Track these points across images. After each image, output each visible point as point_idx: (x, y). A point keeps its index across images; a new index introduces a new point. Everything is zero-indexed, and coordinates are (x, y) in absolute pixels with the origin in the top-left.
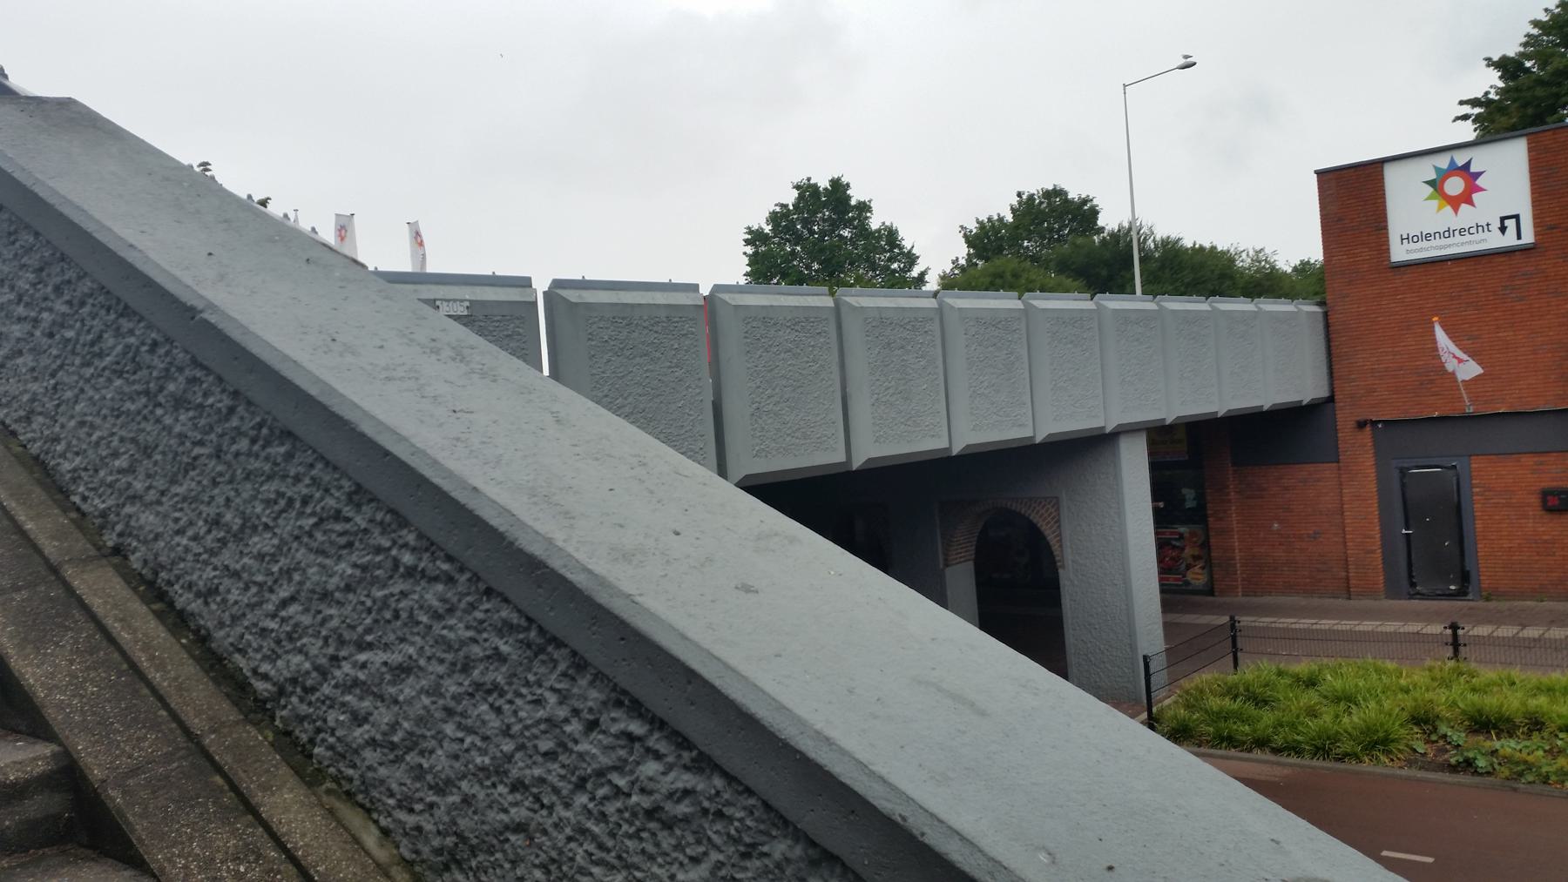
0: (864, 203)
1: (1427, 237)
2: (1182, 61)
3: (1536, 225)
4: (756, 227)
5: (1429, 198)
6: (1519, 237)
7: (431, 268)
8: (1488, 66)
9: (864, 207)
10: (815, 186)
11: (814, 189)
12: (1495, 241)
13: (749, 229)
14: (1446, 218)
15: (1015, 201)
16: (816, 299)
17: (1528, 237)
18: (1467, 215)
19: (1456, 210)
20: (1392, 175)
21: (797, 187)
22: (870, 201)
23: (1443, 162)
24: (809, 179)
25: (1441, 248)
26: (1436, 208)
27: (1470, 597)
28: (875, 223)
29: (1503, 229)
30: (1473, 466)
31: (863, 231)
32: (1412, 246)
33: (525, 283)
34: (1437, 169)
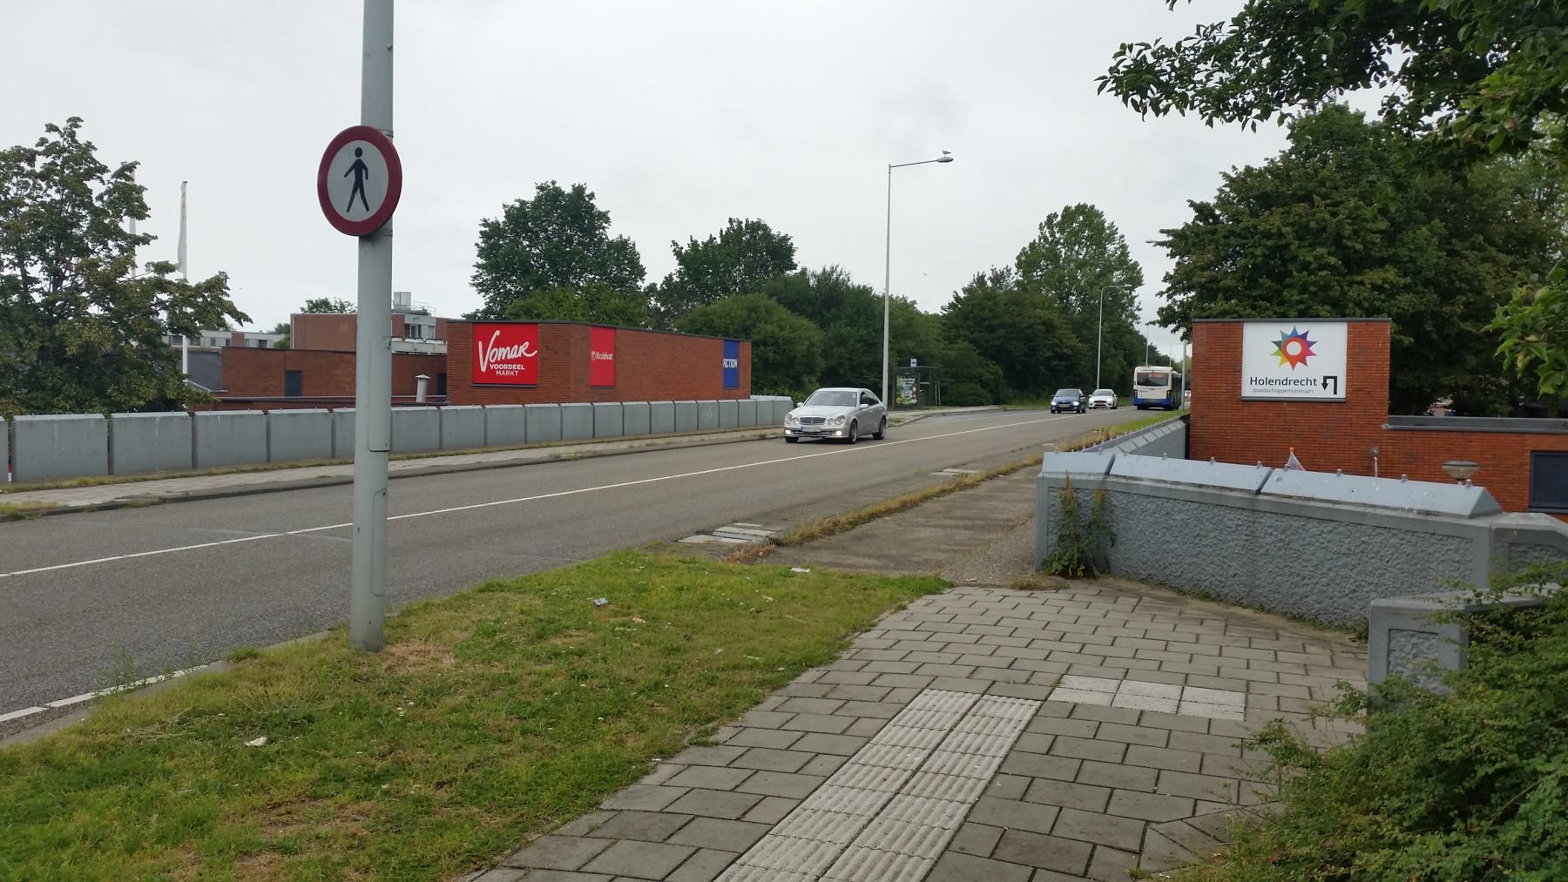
2: (942, 156)
3: (1347, 386)
4: (492, 220)
5: (1275, 354)
6: (1335, 393)
8: (1191, 206)
10: (557, 190)
11: (558, 193)
12: (1318, 393)
13: (485, 223)
14: (1284, 370)
15: (725, 226)
17: (1341, 394)
18: (1300, 371)
19: (1293, 366)
24: (553, 183)
29: (1325, 385)
32: (1258, 387)
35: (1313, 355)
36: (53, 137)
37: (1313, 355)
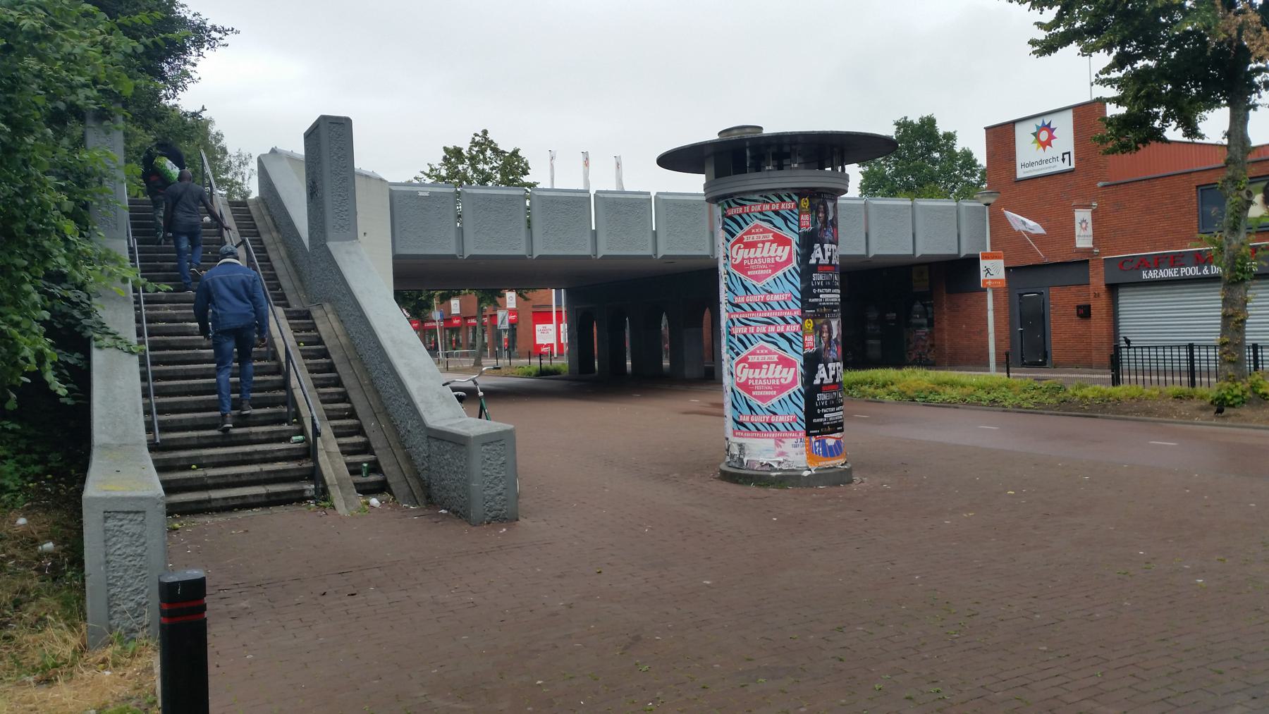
0: (949, 134)
1: (1032, 164)
6: (1070, 165)
7: (555, 188)
9: (950, 137)
14: (1039, 154)
16: (902, 202)
17: (1073, 166)
18: (1050, 152)
20: (1018, 128)
21: (897, 124)
22: (955, 132)
23: (1039, 122)
24: (906, 118)
25: (1038, 170)
26: (1036, 147)
27: (1047, 366)
28: (958, 149)
29: (1063, 160)
30: (1051, 292)
31: (952, 155)
32: (1026, 169)
33: (649, 193)
34: (1037, 126)
35: (1044, 150)
36: (477, 139)
37: (1044, 150)
